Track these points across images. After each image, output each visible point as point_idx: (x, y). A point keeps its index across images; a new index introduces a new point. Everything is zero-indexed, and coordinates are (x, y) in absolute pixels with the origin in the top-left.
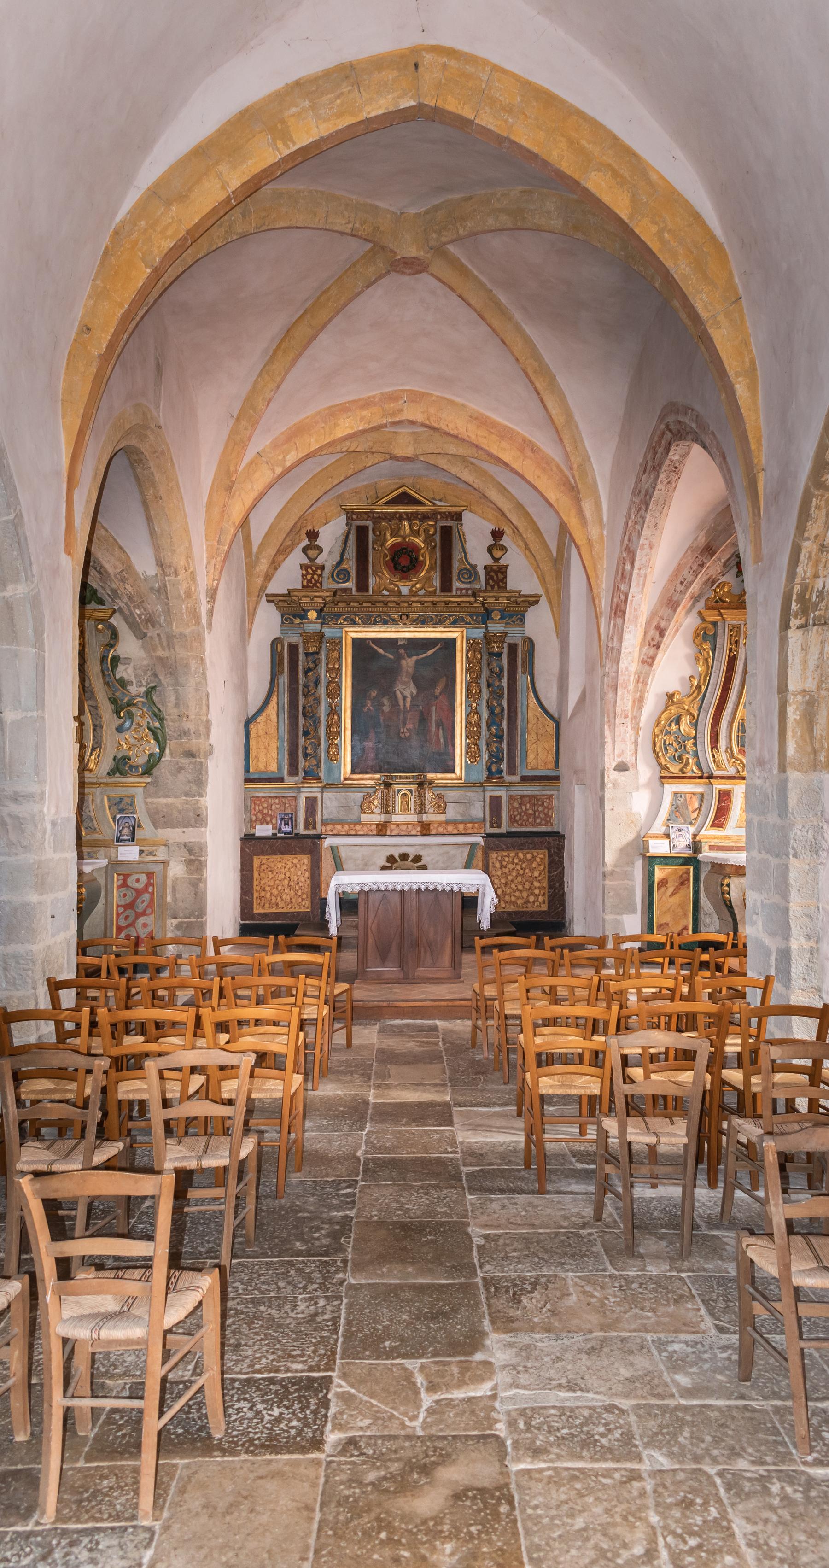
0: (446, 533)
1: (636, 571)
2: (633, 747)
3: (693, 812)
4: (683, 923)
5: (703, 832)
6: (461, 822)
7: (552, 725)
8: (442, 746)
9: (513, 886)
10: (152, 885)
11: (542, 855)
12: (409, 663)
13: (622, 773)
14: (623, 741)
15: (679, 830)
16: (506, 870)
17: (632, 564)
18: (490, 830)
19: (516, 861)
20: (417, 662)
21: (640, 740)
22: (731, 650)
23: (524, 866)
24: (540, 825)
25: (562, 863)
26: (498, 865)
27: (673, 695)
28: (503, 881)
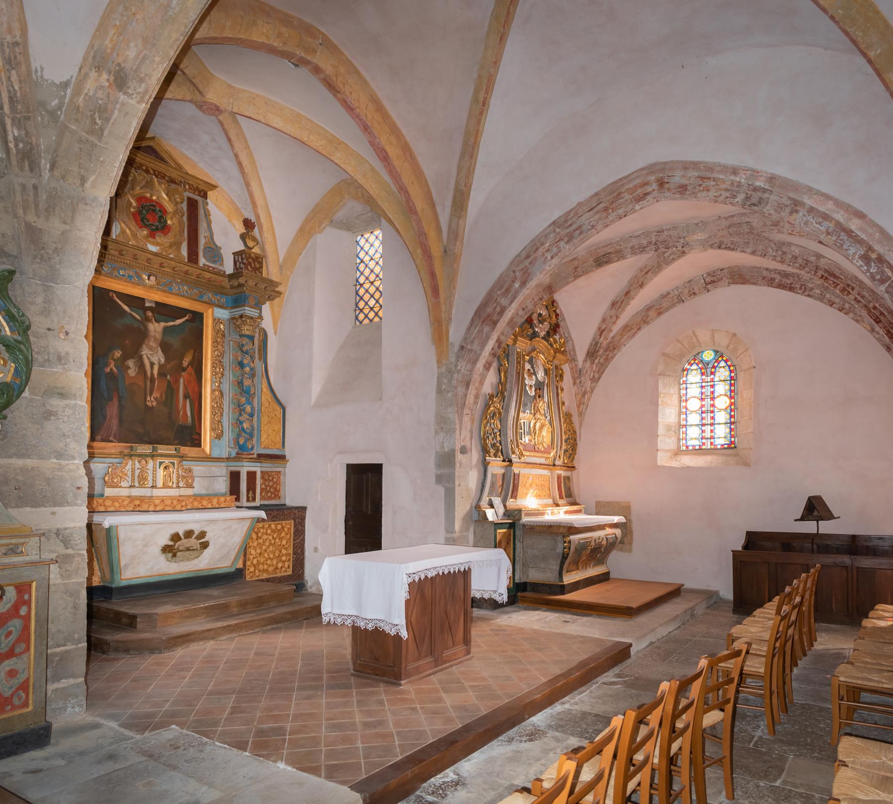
0: (193, 206)
7: (279, 411)
8: (190, 419)
9: (266, 555)
10: (28, 603)
11: (289, 525)
12: (156, 328)
16: (261, 541)
19: (269, 531)
20: (165, 328)
23: (275, 536)
24: (270, 498)
25: (304, 531)
28: (258, 551)
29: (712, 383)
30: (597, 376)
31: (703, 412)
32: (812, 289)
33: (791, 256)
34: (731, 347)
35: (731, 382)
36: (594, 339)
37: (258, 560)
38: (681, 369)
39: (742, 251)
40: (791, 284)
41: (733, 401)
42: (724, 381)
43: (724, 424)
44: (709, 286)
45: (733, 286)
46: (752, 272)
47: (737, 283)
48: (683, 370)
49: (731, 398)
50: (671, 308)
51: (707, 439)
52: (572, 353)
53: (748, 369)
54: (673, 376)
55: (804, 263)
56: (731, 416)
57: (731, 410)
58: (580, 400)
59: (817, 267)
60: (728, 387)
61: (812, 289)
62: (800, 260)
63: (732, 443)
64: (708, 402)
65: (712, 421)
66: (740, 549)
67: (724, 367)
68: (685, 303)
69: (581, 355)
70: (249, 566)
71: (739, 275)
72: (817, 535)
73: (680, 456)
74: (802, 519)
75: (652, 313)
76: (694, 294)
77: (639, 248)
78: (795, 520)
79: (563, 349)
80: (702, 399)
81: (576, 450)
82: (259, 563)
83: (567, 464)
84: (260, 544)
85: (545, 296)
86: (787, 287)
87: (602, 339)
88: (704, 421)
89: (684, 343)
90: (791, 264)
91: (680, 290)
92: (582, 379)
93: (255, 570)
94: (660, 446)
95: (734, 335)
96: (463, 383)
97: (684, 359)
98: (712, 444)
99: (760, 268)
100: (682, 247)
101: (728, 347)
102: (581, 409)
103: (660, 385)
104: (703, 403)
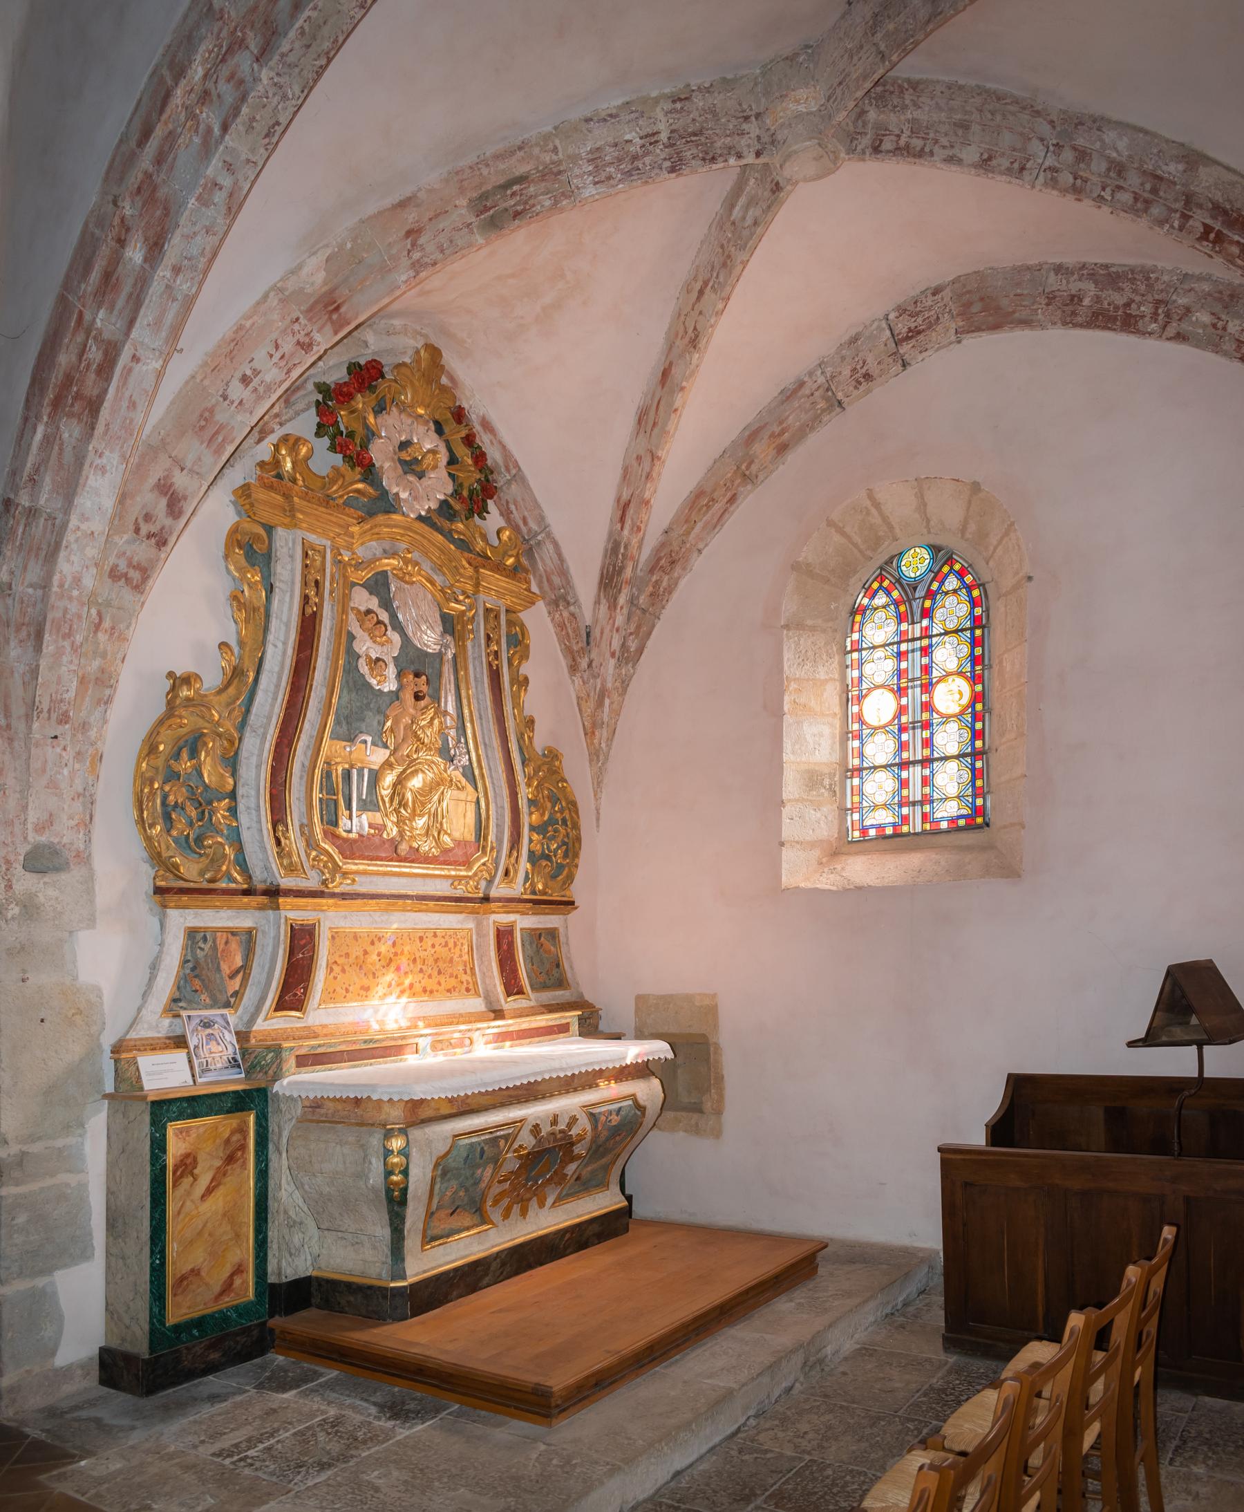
1: (163, 273)
3: (232, 976)
5: (260, 1025)
15: (207, 1024)
17: (156, 248)
22: (306, 599)
29: (925, 642)
30: (633, 645)
31: (902, 729)
32: (1188, 310)
33: (1104, 166)
34: (972, 527)
35: (973, 634)
36: (610, 534)
38: (847, 609)
39: (950, 160)
40: (1128, 305)
41: (979, 688)
42: (956, 631)
43: (957, 757)
44: (905, 349)
45: (970, 341)
46: (1018, 284)
47: (979, 329)
48: (853, 613)
49: (975, 679)
50: (812, 429)
51: (914, 804)
52: (556, 580)
53: (1017, 587)
54: (824, 631)
55: (1148, 186)
56: (977, 735)
57: (976, 717)
58: (593, 716)
59: (1189, 199)
60: (965, 650)
61: (1188, 310)
62: (1133, 180)
63: (979, 811)
64: (915, 696)
65: (927, 752)
66: (978, 1139)
67: (955, 591)
68: (848, 409)
69: (585, 586)
71: (982, 299)
72: (1201, 1082)
73: (844, 858)
74: (1150, 1039)
75: (761, 449)
76: (868, 377)
77: (620, 160)
78: (1131, 1044)
79: (510, 561)
80: (899, 688)
81: (576, 855)
83: (544, 893)
85: (317, 337)
86: (1115, 319)
87: (626, 532)
88: (905, 755)
89: (848, 529)
90: (1107, 195)
91: (829, 370)
92: (594, 655)
94: (789, 830)
95: (976, 487)
96: (24, 634)
97: (852, 581)
98: (925, 817)
99: (1039, 267)
100: (758, 154)
101: (963, 530)
102: (596, 741)
103: (787, 655)
104: (904, 701)
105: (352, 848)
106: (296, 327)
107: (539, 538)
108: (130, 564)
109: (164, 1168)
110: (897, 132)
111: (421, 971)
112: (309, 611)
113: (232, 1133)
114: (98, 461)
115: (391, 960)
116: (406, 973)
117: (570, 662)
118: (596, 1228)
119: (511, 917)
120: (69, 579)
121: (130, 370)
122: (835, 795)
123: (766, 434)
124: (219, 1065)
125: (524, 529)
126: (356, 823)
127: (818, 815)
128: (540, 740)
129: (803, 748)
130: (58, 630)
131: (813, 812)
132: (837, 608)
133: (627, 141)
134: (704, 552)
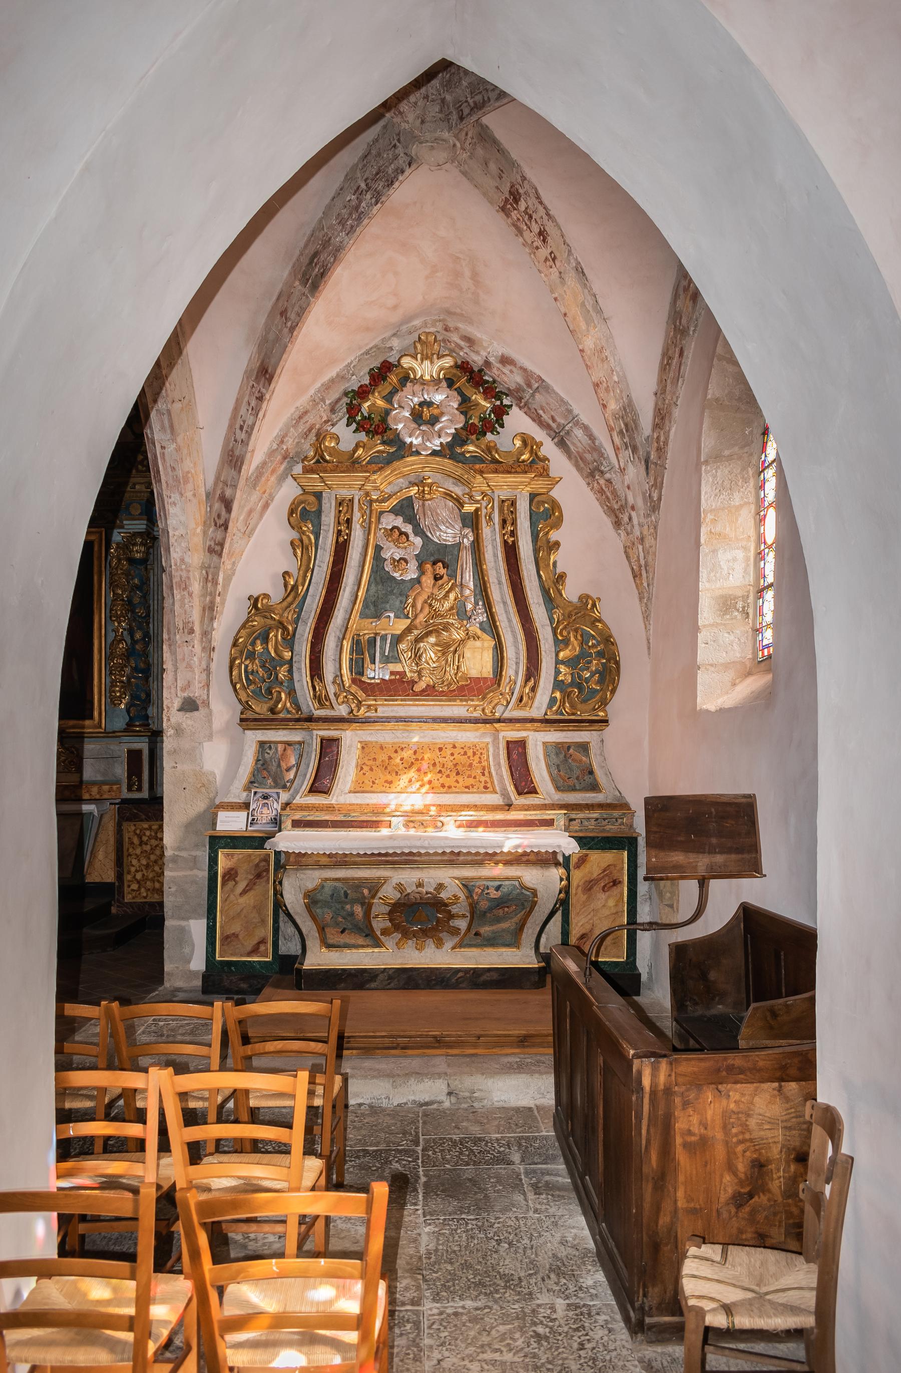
2: (204, 676)
4: (260, 933)
6: (104, 783)
13: (188, 715)
14: (189, 667)
16: (148, 848)
18: (125, 794)
21: (213, 666)
22: (339, 532)
26: (136, 841)
27: (256, 600)
28: (144, 862)
37: (143, 875)
54: (740, 458)
70: (129, 881)
77: (351, 214)
82: (145, 878)
84: (146, 851)
93: (139, 887)
105: (371, 689)
106: (254, 390)
107: (567, 428)
108: (216, 544)
109: (216, 873)
110: (464, 99)
111: (440, 772)
112: (341, 539)
113: (261, 861)
114: (170, 501)
115: (412, 763)
116: (425, 773)
117: (614, 519)
118: (495, 976)
119: (523, 734)
120: (178, 560)
121: (163, 454)
122: (748, 617)
123: (681, 292)
124: (264, 821)
125: (554, 425)
126: (377, 673)
127: (732, 638)
128: (571, 592)
129: (718, 575)
130: (180, 586)
131: (726, 635)
132: (751, 433)
133: (349, 201)
134: (678, 403)
